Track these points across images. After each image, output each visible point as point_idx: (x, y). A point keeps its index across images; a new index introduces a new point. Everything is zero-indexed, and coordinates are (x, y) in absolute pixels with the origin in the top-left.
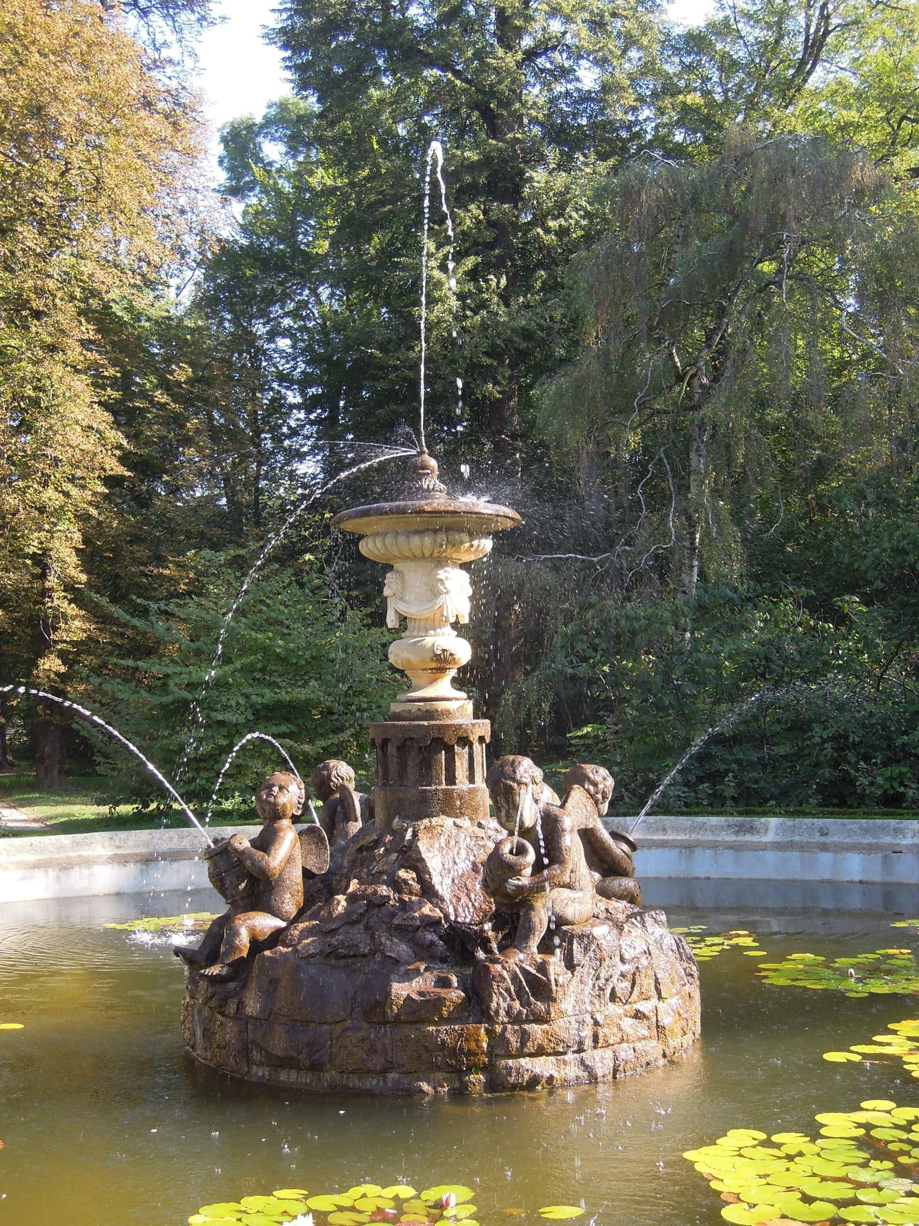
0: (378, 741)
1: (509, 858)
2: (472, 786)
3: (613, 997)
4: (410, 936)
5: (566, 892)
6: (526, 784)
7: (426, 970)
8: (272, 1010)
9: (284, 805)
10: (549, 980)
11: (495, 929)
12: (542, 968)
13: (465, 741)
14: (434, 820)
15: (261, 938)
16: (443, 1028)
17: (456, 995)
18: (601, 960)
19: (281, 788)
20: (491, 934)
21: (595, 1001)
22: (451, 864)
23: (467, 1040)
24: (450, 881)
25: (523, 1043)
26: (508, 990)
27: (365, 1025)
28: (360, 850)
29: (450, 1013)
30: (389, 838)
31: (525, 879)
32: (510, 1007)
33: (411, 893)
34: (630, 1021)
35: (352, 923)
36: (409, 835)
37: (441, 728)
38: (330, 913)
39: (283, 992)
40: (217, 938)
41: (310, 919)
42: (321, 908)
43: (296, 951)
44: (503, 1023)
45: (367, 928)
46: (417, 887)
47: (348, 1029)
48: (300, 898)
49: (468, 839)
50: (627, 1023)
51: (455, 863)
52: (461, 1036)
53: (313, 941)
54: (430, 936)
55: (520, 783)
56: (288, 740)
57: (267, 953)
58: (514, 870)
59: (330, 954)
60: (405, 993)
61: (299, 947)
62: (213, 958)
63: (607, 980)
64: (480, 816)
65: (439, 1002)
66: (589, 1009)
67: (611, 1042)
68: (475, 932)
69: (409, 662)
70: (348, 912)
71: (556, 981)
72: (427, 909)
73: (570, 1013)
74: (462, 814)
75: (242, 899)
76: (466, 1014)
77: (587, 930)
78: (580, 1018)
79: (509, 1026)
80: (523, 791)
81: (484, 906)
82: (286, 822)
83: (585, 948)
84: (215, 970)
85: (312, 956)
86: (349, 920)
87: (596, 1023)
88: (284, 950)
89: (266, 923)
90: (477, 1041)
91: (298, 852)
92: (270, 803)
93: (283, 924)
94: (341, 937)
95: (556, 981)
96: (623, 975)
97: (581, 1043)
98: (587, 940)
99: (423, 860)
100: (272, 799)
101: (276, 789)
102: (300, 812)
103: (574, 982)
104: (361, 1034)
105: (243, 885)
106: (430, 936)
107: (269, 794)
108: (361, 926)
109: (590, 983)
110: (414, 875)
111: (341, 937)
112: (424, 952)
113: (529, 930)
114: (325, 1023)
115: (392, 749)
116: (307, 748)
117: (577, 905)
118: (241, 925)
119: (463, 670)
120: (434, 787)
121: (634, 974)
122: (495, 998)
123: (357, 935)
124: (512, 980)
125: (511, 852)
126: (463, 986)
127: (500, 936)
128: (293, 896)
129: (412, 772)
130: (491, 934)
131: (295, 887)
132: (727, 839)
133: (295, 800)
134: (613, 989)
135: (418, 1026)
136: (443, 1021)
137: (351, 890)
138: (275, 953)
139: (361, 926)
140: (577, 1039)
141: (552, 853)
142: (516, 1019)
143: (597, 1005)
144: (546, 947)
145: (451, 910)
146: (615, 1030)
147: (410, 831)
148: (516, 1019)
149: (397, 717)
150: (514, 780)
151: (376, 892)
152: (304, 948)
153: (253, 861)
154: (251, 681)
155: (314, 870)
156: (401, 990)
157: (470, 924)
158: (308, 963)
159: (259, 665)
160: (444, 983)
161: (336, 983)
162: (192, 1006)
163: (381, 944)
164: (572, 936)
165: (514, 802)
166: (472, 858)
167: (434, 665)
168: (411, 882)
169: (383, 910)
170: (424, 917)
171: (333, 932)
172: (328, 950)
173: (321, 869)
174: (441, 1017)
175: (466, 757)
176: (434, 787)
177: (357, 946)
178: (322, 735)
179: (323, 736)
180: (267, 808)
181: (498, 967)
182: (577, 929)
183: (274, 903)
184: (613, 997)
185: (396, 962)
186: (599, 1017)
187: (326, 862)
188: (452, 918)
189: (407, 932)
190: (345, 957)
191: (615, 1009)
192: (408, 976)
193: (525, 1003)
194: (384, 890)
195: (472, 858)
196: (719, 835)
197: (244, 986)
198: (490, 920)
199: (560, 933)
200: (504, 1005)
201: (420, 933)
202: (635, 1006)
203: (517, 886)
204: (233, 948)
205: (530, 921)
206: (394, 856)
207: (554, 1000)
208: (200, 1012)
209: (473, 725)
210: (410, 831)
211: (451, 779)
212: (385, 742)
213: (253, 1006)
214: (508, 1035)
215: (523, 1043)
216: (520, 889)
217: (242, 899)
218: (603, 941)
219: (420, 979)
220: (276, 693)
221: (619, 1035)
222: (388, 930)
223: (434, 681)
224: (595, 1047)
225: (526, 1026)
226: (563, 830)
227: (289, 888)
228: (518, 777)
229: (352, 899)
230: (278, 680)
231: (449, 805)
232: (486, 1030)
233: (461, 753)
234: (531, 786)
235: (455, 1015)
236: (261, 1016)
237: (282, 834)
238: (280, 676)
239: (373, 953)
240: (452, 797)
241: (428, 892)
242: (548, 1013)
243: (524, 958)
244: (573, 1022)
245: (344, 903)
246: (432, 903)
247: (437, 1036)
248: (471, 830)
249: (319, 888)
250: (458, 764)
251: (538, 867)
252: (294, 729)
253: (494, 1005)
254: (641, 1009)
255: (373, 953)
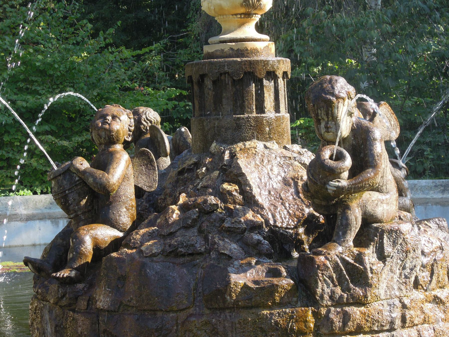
0: (195, 79)
1: (331, 163)
2: (278, 115)
3: (416, 284)
4: (238, 238)
5: (375, 195)
6: (343, 99)
7: (257, 263)
8: (121, 303)
9: (118, 131)
10: (365, 268)
11: (307, 233)
12: (359, 258)
13: (272, 75)
14: (248, 143)
15: (104, 246)
16: (275, 312)
17: (286, 282)
18: (407, 252)
19: (114, 117)
20: (304, 237)
21: (403, 287)
22: (266, 179)
23: (297, 321)
24: (267, 193)
25: (345, 324)
26: (330, 278)
27: (207, 312)
28: (181, 173)
29: (281, 298)
30: (208, 160)
31: (344, 181)
32: (333, 292)
33: (235, 203)
34: (430, 306)
35: (187, 227)
36: (227, 156)
37: (251, 63)
38: (167, 220)
39: (131, 287)
40: (62, 249)
41: (148, 226)
42: (156, 218)
43: (141, 251)
44: (327, 306)
45: (200, 231)
46: (240, 198)
47: (191, 315)
48: (134, 211)
49: (279, 159)
50: (428, 307)
51: (270, 178)
52: (291, 317)
53: (155, 243)
54: (256, 237)
55: (338, 98)
56: (50, 136)
57: (114, 254)
58: (335, 174)
59: (172, 254)
60: (242, 282)
61: (143, 248)
62: (61, 263)
63: (412, 270)
64: (285, 141)
65: (273, 288)
66: (397, 294)
67: (416, 322)
68: (291, 235)
69: (221, 8)
70: (182, 219)
71: (371, 269)
72: (250, 215)
73: (383, 297)
74: (271, 139)
75: (84, 213)
76: (295, 299)
77: (395, 226)
78: (391, 301)
79: (333, 309)
80: (341, 105)
81: (297, 213)
82: (119, 147)
83: (394, 242)
84: (65, 273)
85: (154, 255)
86: (184, 225)
87: (404, 306)
88: (130, 251)
89: (106, 233)
90: (306, 322)
91: (131, 171)
92: (105, 129)
93: (121, 234)
94: (179, 238)
95: (371, 269)
96: (423, 266)
97: (392, 323)
98: (395, 234)
99: (243, 175)
100: (107, 126)
101: (110, 118)
102: (130, 139)
103: (385, 270)
104: (204, 318)
105: (84, 201)
106: (256, 237)
107: (104, 122)
108: (195, 230)
109: (398, 272)
110: (237, 188)
111: (179, 238)
112: (252, 249)
113: (347, 226)
114: (172, 311)
115: (208, 83)
116: (65, 143)
117: (385, 205)
118: (85, 235)
119: (267, 16)
120: (246, 115)
121: (433, 265)
122: (320, 284)
123: (192, 237)
124: (334, 268)
125: (331, 158)
126: (290, 275)
127: (311, 239)
128: (128, 210)
129: (227, 106)
130: (304, 237)
131: (130, 202)
132: (435, 196)
133: (126, 127)
134: (416, 277)
135: (254, 310)
136: (276, 305)
137: (181, 201)
138: (122, 254)
139: (195, 230)
140: (389, 319)
141: (363, 160)
142: (338, 303)
143: (404, 291)
144: (362, 240)
145: (270, 216)
146: (419, 312)
147: (227, 152)
148: (338, 303)
149: (211, 56)
150: (333, 94)
151: (205, 201)
152: (147, 249)
153: (95, 178)
154: (15, 90)
155: (145, 188)
156: (239, 280)
157: (287, 228)
158: (152, 261)
159: (22, 77)
160: (276, 273)
161: (181, 277)
162: (41, 309)
163: (215, 243)
164: (383, 232)
165: (333, 114)
166: (283, 174)
167: (242, 10)
168: (234, 193)
169: (214, 216)
170: (248, 222)
171: (171, 235)
172: (169, 250)
173: (151, 187)
174: (274, 303)
175: (273, 90)
176: (246, 115)
177: (193, 245)
178: (77, 133)
179: (79, 133)
180: (103, 134)
181: (322, 258)
182: (387, 226)
183: (112, 216)
184: (416, 284)
185: (229, 258)
186: (406, 301)
187: (155, 181)
188: (272, 222)
189: (238, 233)
190: (183, 255)
191: (419, 295)
192: (242, 269)
193: (345, 289)
194: (212, 200)
195: (283, 174)
196: (428, 194)
197: (91, 286)
198: (303, 225)
199: (370, 231)
200: (327, 290)
201: (246, 234)
202: (433, 293)
203: (338, 187)
204: (80, 255)
205: (347, 219)
206: (216, 173)
207: (370, 286)
208: (50, 311)
209: (279, 61)
210: (227, 152)
211: (261, 109)
212: (203, 77)
213: (103, 300)
214: (332, 316)
215: (345, 324)
216: (340, 190)
217: (84, 213)
218: (408, 236)
219: (253, 271)
220: (37, 99)
221: (422, 317)
222: (220, 232)
223: (241, 25)
224: (403, 327)
225: (347, 309)
226: (375, 140)
227: (124, 203)
228: (337, 92)
229: (184, 208)
230: (39, 88)
231: (259, 131)
232: (313, 312)
233: (268, 85)
234: (347, 100)
235: (286, 300)
236: (112, 308)
237: (118, 156)
238: (39, 85)
239: (208, 251)
240: (262, 124)
241: (250, 201)
242: (366, 296)
243: (342, 251)
244: (385, 305)
245: (177, 212)
246: (253, 211)
247: (271, 318)
248: (279, 151)
249: (149, 204)
250: (266, 95)
251: (355, 172)
252: (54, 128)
253: (319, 290)
254: (439, 295)
255: (208, 251)
